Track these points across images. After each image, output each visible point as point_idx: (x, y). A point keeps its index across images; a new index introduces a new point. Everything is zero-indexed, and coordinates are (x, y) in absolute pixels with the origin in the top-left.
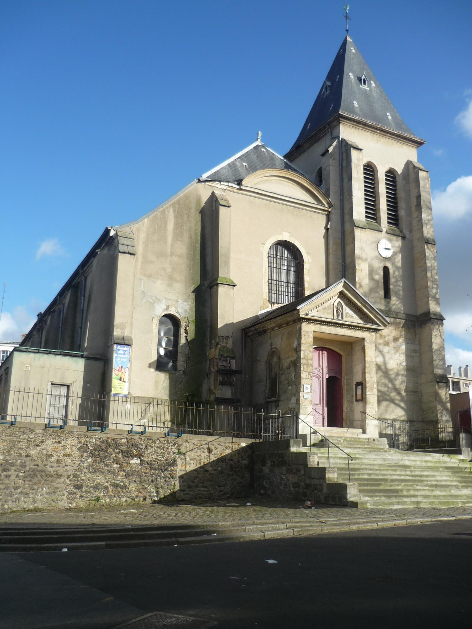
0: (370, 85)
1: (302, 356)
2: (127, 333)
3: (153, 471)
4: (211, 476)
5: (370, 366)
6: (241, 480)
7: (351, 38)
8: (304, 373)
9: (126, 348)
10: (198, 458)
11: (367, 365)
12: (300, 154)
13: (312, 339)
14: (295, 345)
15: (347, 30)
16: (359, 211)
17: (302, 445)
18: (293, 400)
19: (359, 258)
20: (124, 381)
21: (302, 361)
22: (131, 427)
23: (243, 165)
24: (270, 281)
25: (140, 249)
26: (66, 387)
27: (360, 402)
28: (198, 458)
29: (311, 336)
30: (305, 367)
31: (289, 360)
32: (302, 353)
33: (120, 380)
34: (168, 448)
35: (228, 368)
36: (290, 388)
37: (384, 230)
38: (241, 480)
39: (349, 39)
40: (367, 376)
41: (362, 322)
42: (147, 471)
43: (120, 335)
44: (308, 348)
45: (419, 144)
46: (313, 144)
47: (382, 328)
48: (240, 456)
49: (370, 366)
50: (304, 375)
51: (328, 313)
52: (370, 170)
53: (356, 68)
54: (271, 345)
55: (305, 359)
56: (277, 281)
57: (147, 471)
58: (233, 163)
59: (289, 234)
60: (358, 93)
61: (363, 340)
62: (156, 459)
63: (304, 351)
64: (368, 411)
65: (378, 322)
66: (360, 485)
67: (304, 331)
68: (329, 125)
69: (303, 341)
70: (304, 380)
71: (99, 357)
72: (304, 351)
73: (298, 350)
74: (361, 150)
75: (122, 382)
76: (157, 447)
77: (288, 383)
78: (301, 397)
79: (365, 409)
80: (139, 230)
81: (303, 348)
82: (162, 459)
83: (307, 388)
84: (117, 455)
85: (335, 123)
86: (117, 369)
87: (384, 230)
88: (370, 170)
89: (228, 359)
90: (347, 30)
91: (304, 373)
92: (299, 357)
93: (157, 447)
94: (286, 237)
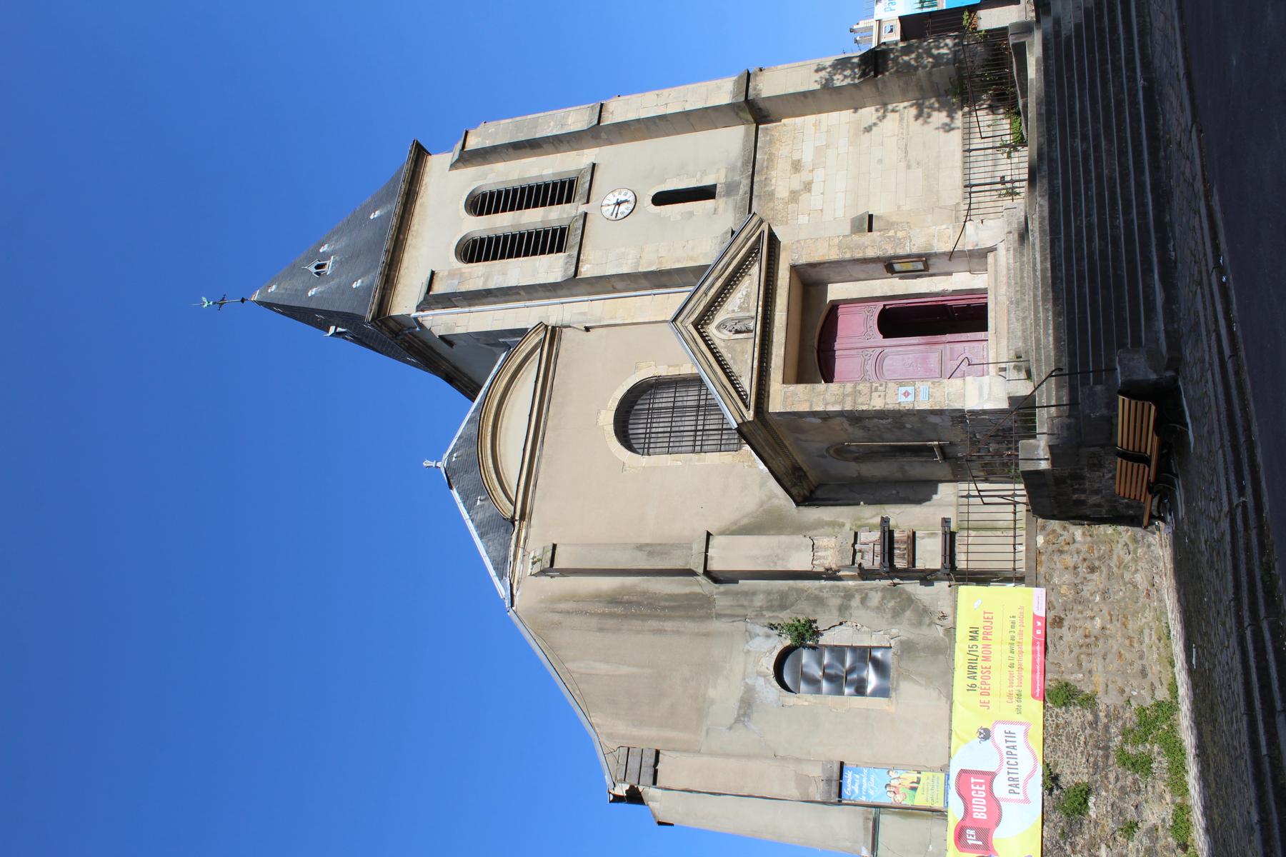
0: (326, 256)
1: (837, 408)
2: (816, 772)
3: (1111, 762)
4: (1114, 618)
5: (849, 248)
6: (1120, 546)
7: (254, 292)
8: (873, 403)
9: (848, 775)
10: (1076, 651)
11: (848, 256)
12: (464, 374)
13: (801, 388)
14: (817, 421)
15: (243, 300)
16: (548, 268)
17: (1032, 441)
18: (933, 419)
19: (638, 263)
20: (918, 782)
21: (848, 407)
22: (1019, 507)
23: (482, 506)
24: (698, 448)
25: (647, 736)
26: (961, 564)
27: (930, 262)
28: (1076, 651)
29: (793, 388)
30: (860, 400)
31: (850, 429)
32: (830, 408)
33: (914, 789)
34: (1057, 726)
35: (878, 548)
36: (908, 426)
37: (583, 208)
38: (1120, 546)
39: (255, 297)
40: (871, 253)
41: (757, 265)
42: (1112, 777)
43: (822, 785)
44: (819, 394)
45: (420, 153)
46: (439, 355)
47: (765, 227)
48: (1066, 548)
49: (849, 248)
50: (877, 403)
51: (743, 352)
52: (473, 251)
53: (298, 283)
54: (824, 457)
55: (842, 402)
56: (696, 431)
57: (1112, 777)
58: (477, 527)
59: (603, 412)
60: (337, 279)
61: (794, 269)
62: (1082, 753)
63: (826, 404)
64: (947, 247)
65: (753, 239)
66: (1121, 345)
67: (785, 406)
68: (397, 334)
69: (804, 407)
70: (888, 400)
71: (871, 824)
72: (826, 404)
73: (826, 416)
74: (433, 273)
75: (920, 786)
76: (1054, 750)
77: (900, 428)
78: (927, 407)
79: (944, 254)
80: (610, 736)
81: (819, 407)
82: (1082, 738)
83: (906, 394)
84: (1078, 848)
85: (392, 324)
86: (892, 795)
87: (583, 208)
88: (473, 251)
89: (857, 547)
90: (243, 300)
91: (873, 403)
92: (841, 414)
93: (1054, 750)
94: (607, 419)
